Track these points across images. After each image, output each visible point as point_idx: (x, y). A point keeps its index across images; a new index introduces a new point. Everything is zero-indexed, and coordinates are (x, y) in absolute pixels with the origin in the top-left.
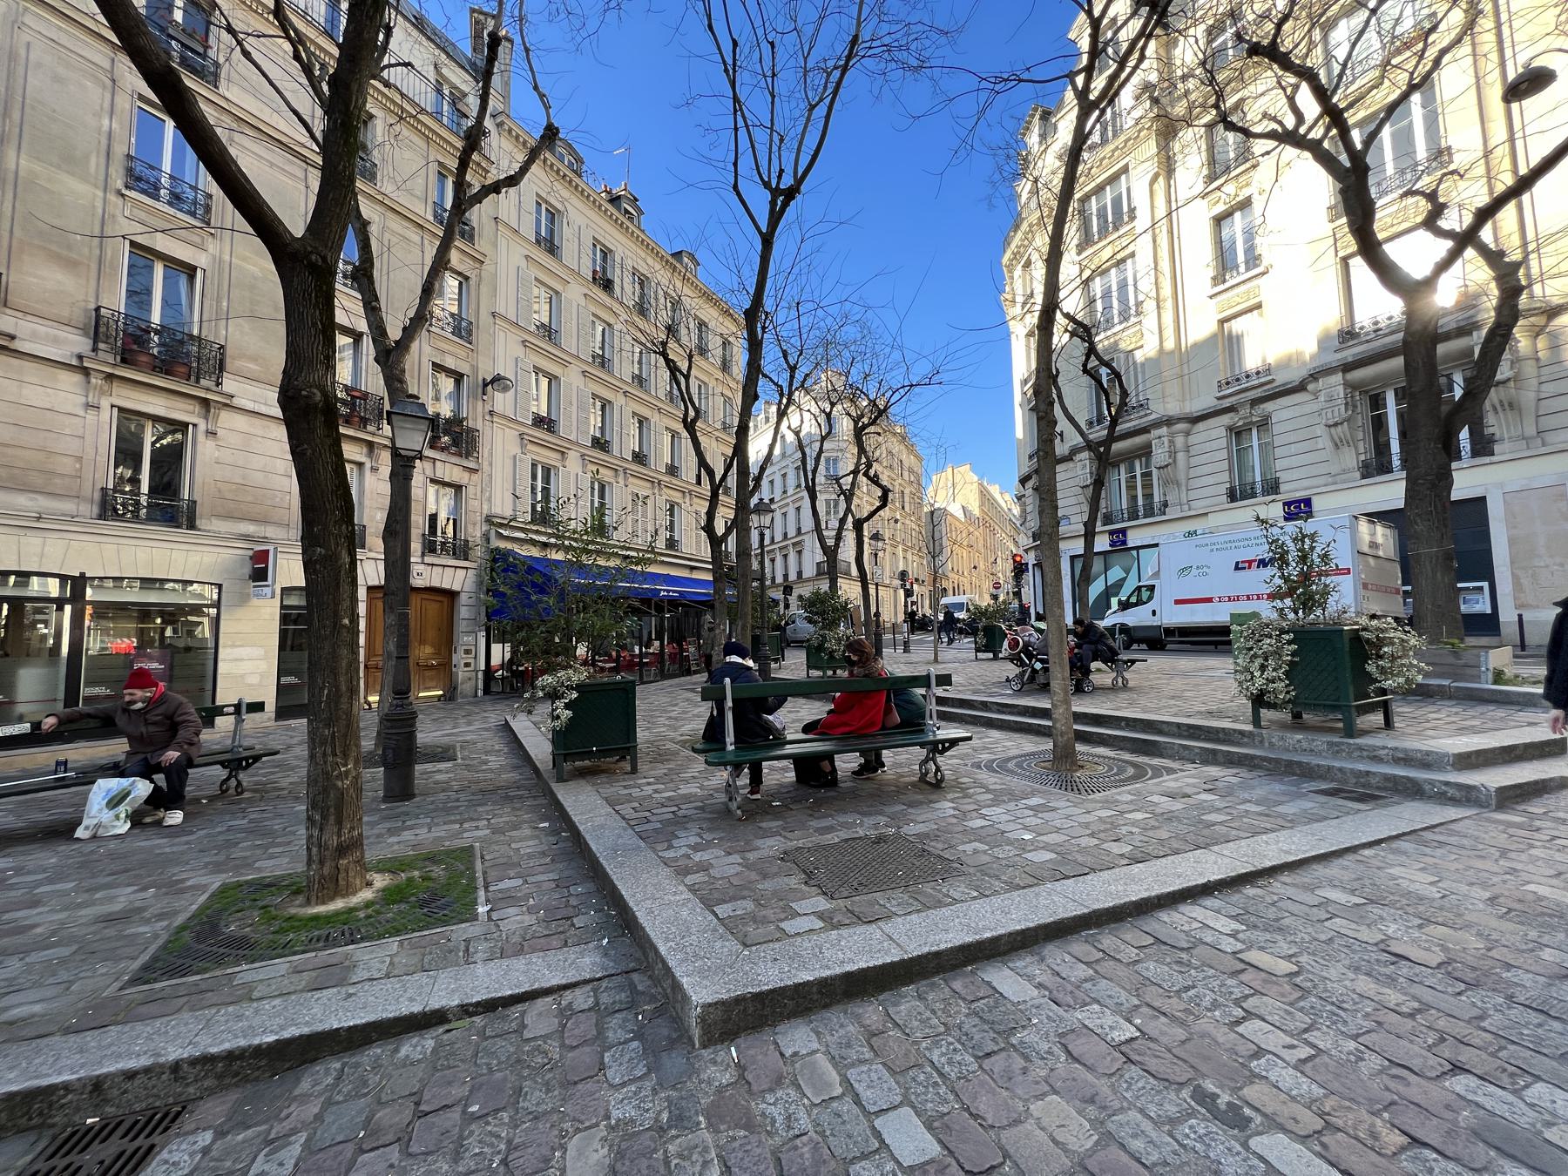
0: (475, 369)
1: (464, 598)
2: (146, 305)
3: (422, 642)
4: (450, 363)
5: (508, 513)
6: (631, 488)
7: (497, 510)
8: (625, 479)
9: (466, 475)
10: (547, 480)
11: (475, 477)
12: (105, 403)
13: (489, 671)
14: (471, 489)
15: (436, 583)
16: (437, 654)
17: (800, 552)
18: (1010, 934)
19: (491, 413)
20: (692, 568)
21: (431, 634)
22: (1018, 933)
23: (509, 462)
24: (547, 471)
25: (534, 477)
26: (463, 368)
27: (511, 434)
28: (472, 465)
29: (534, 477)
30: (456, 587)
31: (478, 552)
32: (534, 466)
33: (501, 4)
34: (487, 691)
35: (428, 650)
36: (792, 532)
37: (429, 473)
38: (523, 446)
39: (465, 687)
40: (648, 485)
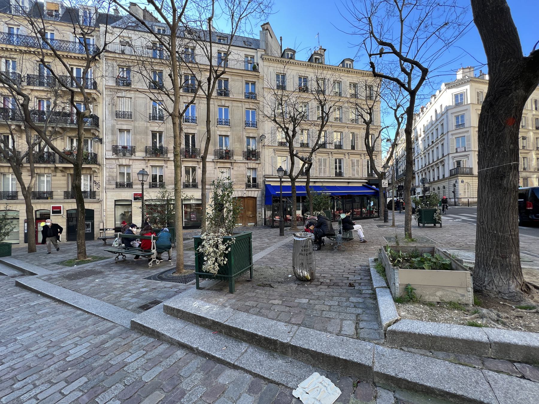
0: (258, 134)
1: (258, 199)
2: (222, 146)
3: (248, 211)
4: (251, 135)
5: (271, 174)
6: (351, 158)
7: (267, 173)
8: (332, 155)
9: (257, 165)
10: (340, 163)
11: (260, 165)
12: (149, 165)
13: (265, 219)
14: (259, 169)
15: (249, 195)
16: (253, 214)
17: (444, 165)
18: (422, 385)
19: (264, 146)
20: (349, 182)
21: (251, 208)
22: (426, 387)
23: (270, 159)
24: (340, 161)
25: (336, 163)
26: (255, 135)
27: (271, 150)
28: (258, 162)
29: (336, 163)
30: (256, 196)
31: (262, 186)
32: (336, 160)
33: (1, 57)
34: (265, 224)
35: (250, 213)
36: (440, 157)
37: (247, 167)
38: (275, 153)
39: (259, 223)
40: (327, 154)
